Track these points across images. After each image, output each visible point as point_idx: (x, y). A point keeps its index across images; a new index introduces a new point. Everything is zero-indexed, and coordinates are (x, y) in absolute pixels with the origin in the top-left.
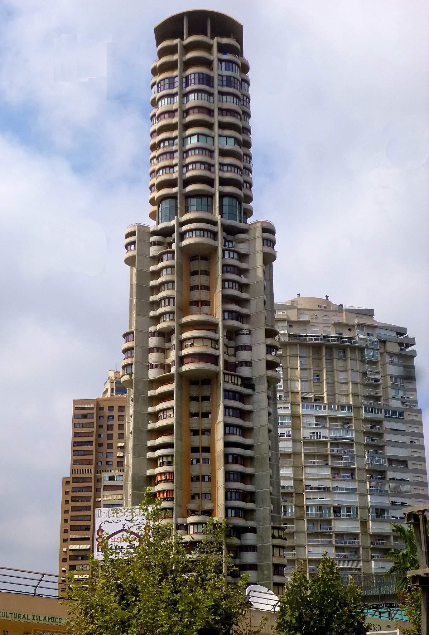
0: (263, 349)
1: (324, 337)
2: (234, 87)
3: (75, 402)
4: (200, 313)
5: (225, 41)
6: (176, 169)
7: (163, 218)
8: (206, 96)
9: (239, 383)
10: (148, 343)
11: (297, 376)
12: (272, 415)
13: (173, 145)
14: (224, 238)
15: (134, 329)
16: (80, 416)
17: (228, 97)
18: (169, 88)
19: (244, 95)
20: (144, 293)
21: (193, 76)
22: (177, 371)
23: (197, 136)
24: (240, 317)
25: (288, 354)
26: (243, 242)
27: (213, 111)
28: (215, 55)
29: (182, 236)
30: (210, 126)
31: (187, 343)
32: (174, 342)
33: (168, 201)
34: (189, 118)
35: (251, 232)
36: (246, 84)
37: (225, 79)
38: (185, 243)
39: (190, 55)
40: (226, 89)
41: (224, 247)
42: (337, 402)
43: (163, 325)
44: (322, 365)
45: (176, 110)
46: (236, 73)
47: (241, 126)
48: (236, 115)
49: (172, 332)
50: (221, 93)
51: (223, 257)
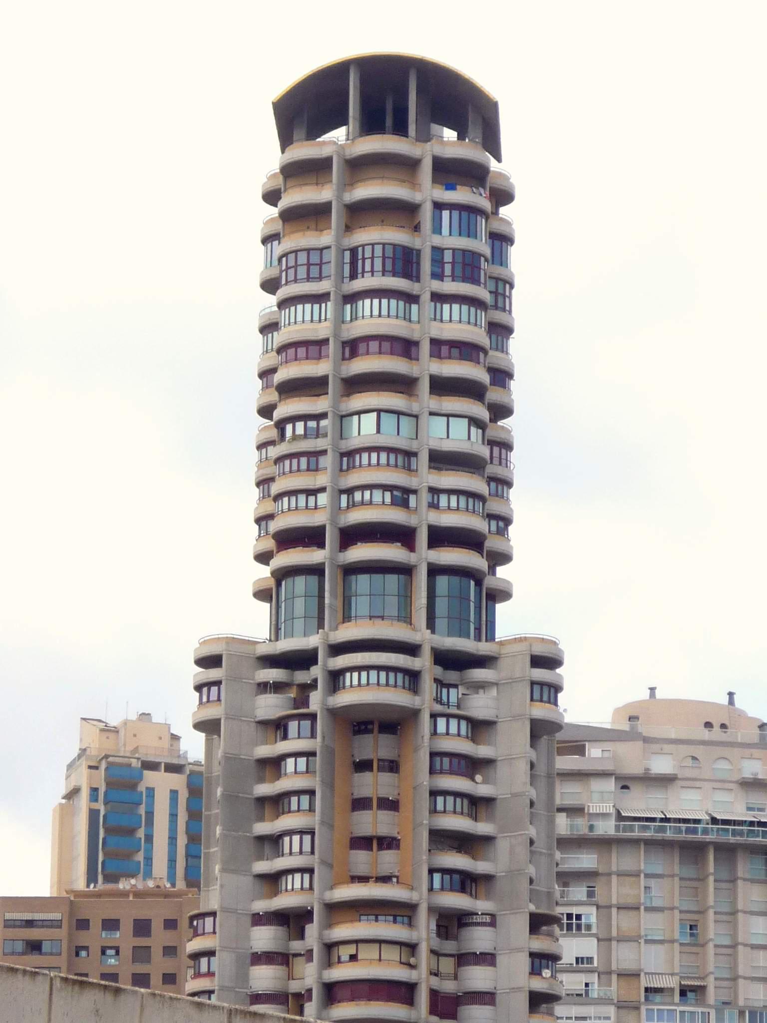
0: (524, 963)
14: (436, 680)
16: (20, 947)
17: (456, 307)
28: (426, 191)
35: (503, 663)
39: (366, 191)
40: (449, 287)
41: (438, 708)
42: (741, 1003)
43: (287, 900)
44: (705, 897)
51: (434, 733)
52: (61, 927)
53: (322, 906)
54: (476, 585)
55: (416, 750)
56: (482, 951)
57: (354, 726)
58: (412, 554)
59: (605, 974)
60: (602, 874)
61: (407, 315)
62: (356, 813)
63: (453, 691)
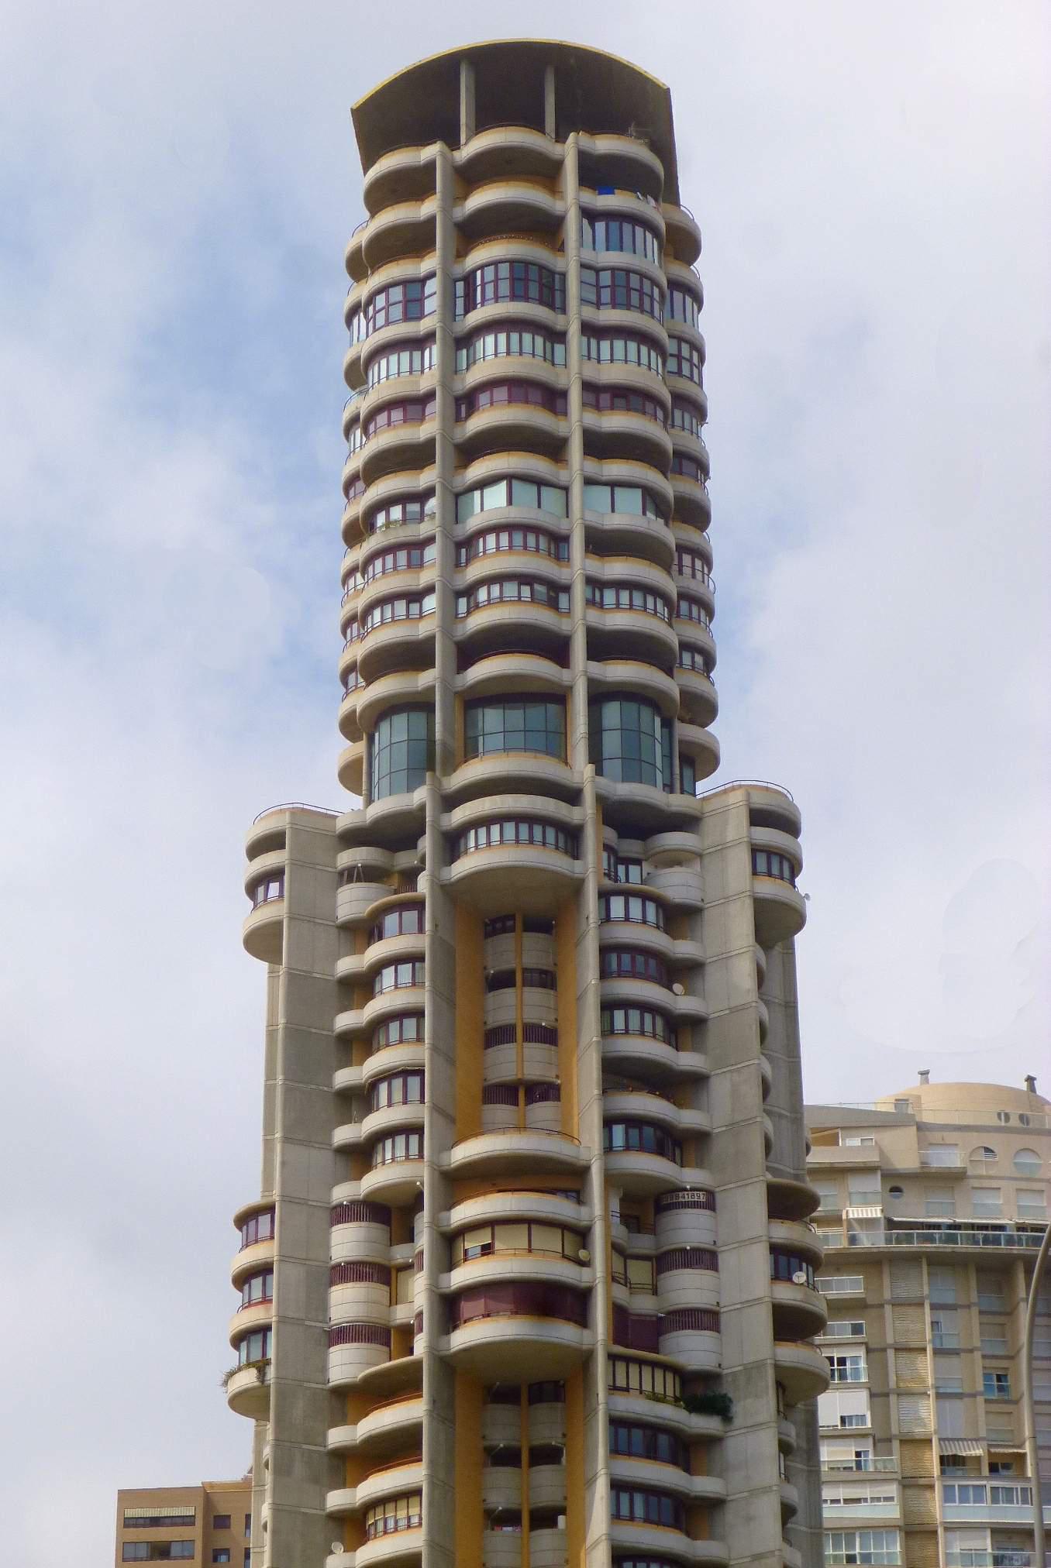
0: (760, 1262)
1: (1021, 1228)
2: (642, 310)
3: (126, 1497)
4: (521, 1127)
5: (605, 144)
6: (431, 603)
7: (385, 782)
8: (539, 340)
9: (670, 1392)
10: (327, 1246)
11: (923, 1381)
12: (800, 1516)
13: (421, 517)
14: (607, 848)
15: (276, 1196)
16: (143, 1551)
17: (619, 344)
18: (407, 318)
19: (680, 339)
20: (318, 1062)
21: (490, 272)
22: (432, 1349)
23: (503, 485)
24: (673, 1142)
25: (887, 1295)
26: (679, 863)
27: (564, 394)
28: (570, 198)
29: (453, 844)
30: (553, 448)
31: (473, 1243)
32: (424, 1240)
33: (400, 721)
34: (477, 423)
35: (708, 825)
36: (689, 300)
37: (606, 278)
38: (462, 867)
39: (482, 198)
41: (608, 883)
43: (386, 1173)
44: (1016, 1333)
45: (430, 396)
46: (647, 257)
47: (670, 448)
48: (649, 407)
49: (415, 1203)
50: (590, 330)
51: (606, 919)
52: (193, 1524)
53: (437, 1174)
54: (662, 726)
55: (578, 942)
56: (696, 1245)
57: (486, 925)
58: (565, 671)
59: (882, 1441)
60: (872, 1306)
61: (548, 356)
62: (490, 1050)
63: (634, 870)
